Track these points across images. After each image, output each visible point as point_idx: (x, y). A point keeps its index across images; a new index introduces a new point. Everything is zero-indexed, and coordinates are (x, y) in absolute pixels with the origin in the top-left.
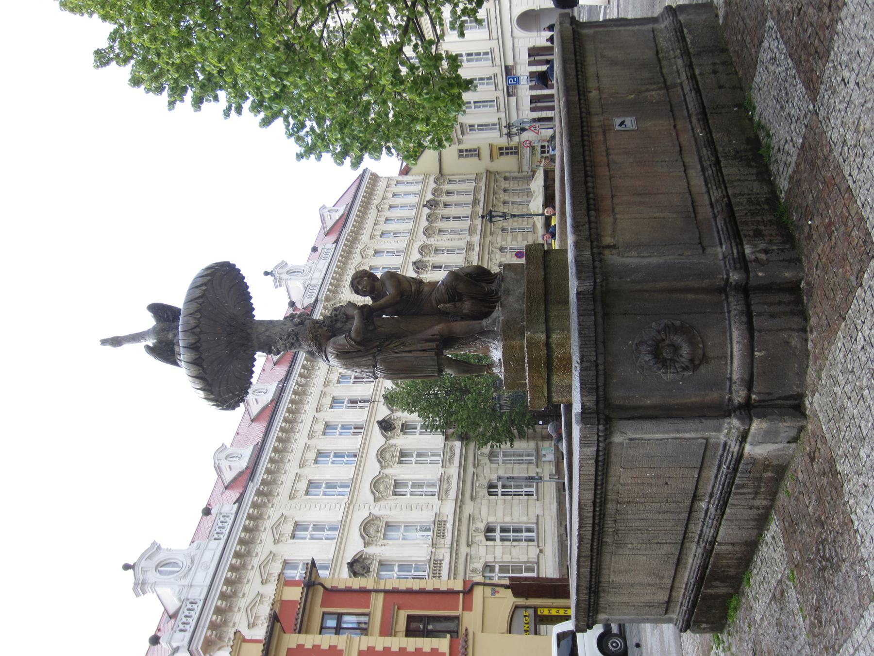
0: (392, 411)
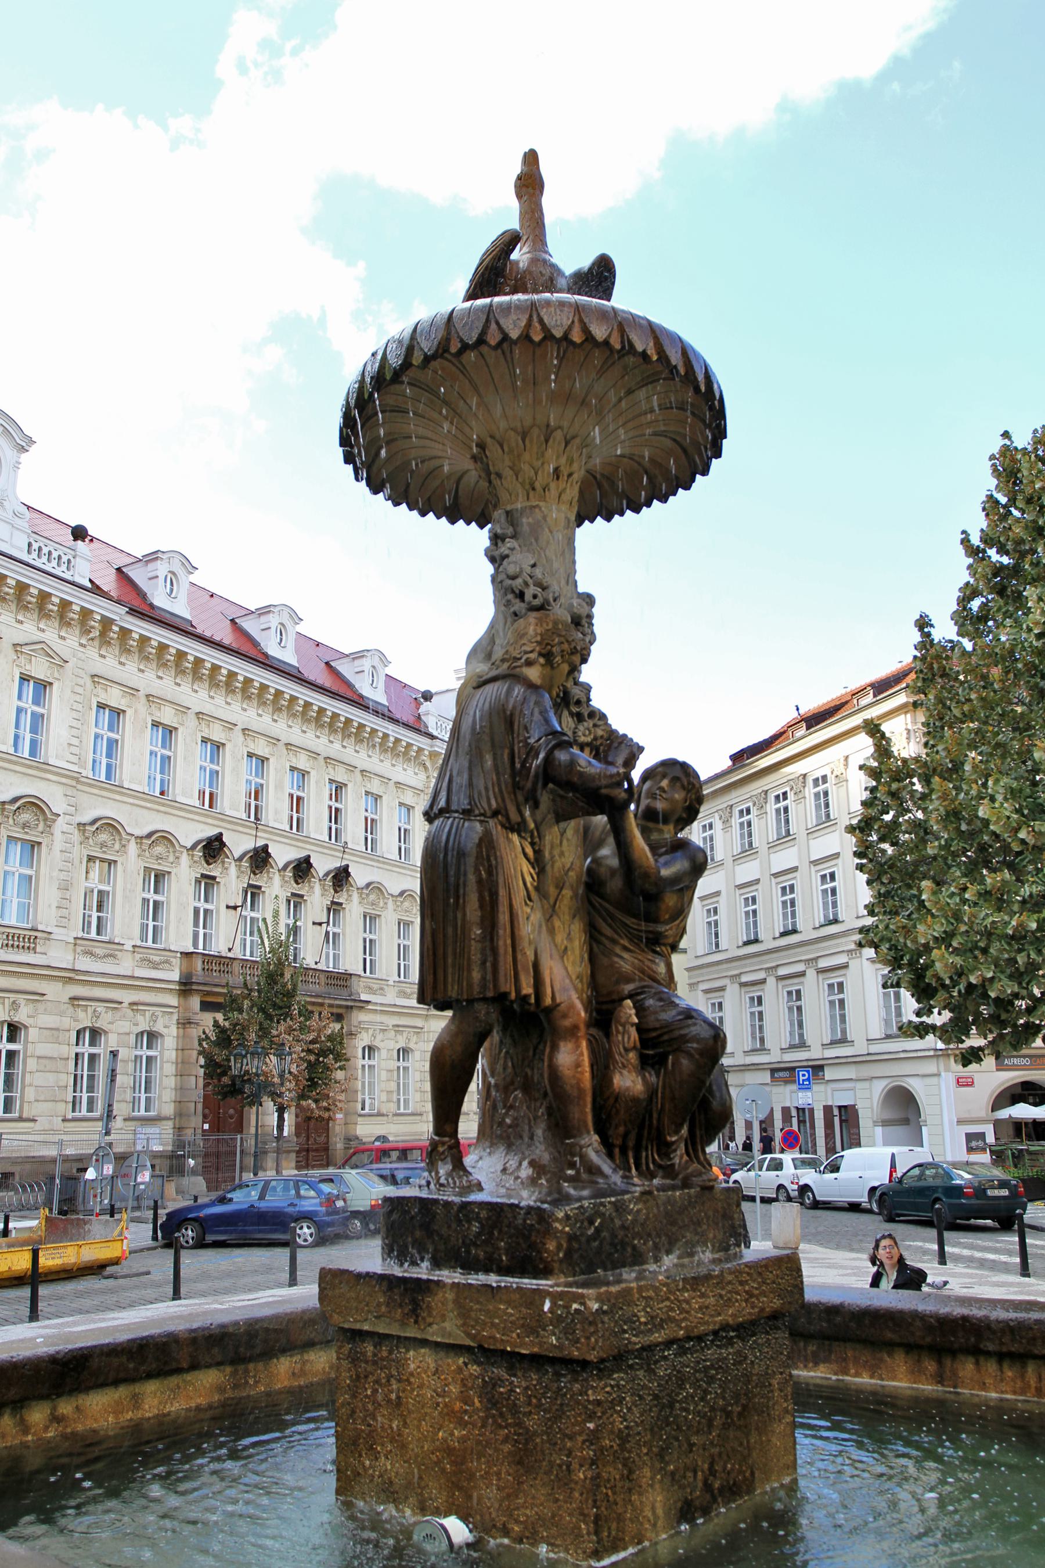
0: (240, 859)
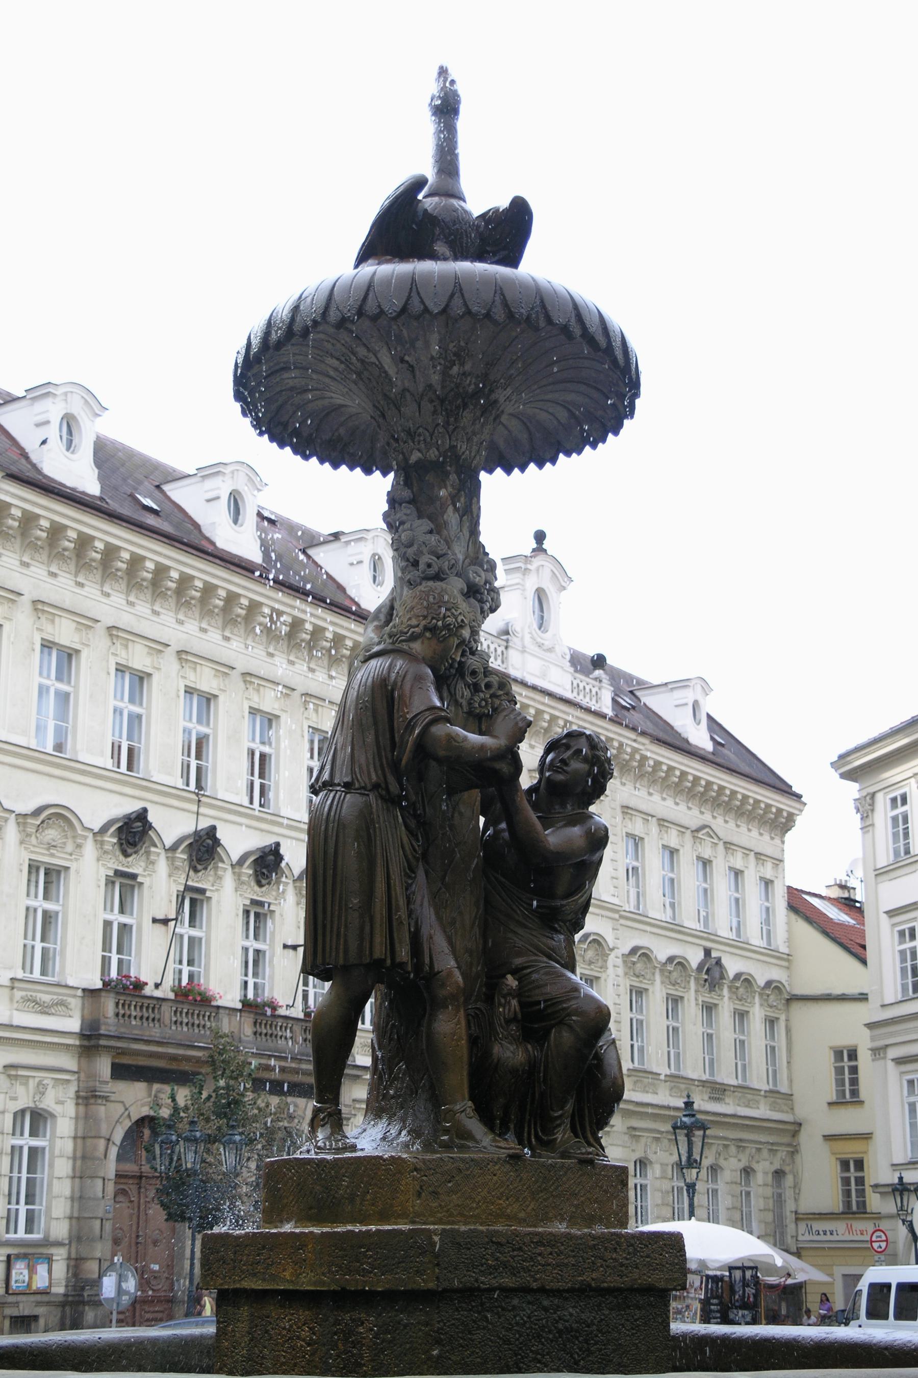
0: (174, 848)
